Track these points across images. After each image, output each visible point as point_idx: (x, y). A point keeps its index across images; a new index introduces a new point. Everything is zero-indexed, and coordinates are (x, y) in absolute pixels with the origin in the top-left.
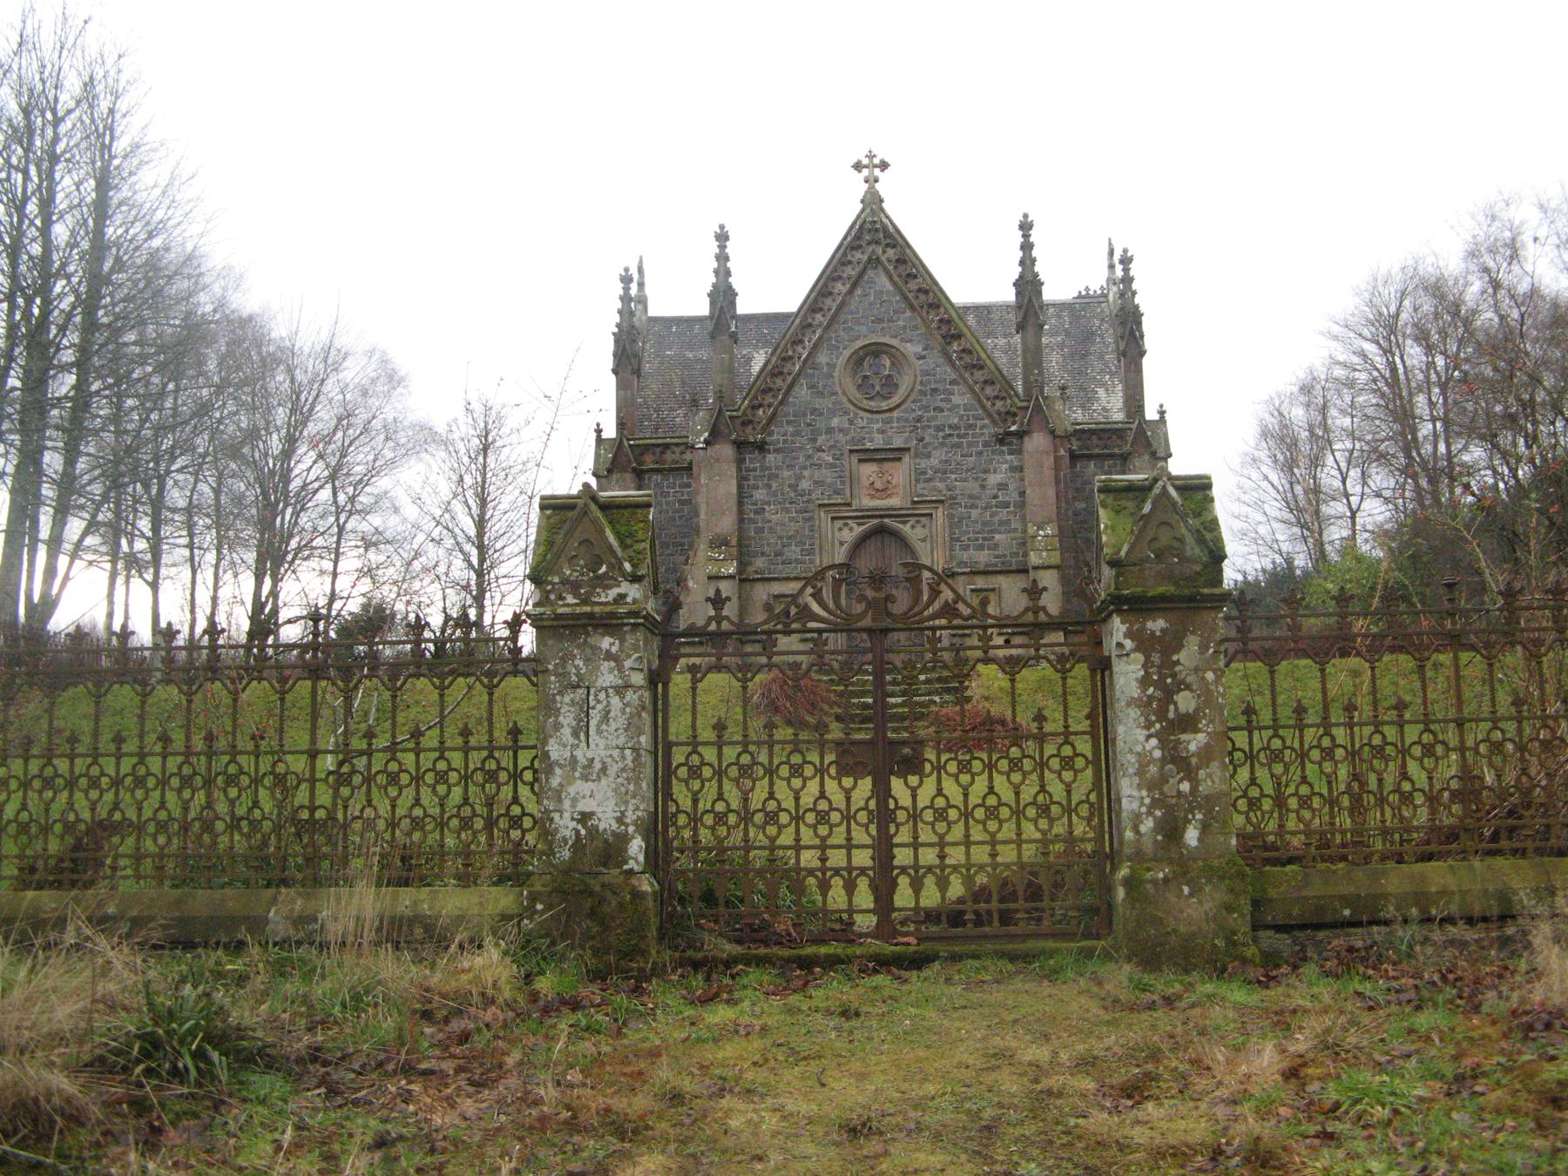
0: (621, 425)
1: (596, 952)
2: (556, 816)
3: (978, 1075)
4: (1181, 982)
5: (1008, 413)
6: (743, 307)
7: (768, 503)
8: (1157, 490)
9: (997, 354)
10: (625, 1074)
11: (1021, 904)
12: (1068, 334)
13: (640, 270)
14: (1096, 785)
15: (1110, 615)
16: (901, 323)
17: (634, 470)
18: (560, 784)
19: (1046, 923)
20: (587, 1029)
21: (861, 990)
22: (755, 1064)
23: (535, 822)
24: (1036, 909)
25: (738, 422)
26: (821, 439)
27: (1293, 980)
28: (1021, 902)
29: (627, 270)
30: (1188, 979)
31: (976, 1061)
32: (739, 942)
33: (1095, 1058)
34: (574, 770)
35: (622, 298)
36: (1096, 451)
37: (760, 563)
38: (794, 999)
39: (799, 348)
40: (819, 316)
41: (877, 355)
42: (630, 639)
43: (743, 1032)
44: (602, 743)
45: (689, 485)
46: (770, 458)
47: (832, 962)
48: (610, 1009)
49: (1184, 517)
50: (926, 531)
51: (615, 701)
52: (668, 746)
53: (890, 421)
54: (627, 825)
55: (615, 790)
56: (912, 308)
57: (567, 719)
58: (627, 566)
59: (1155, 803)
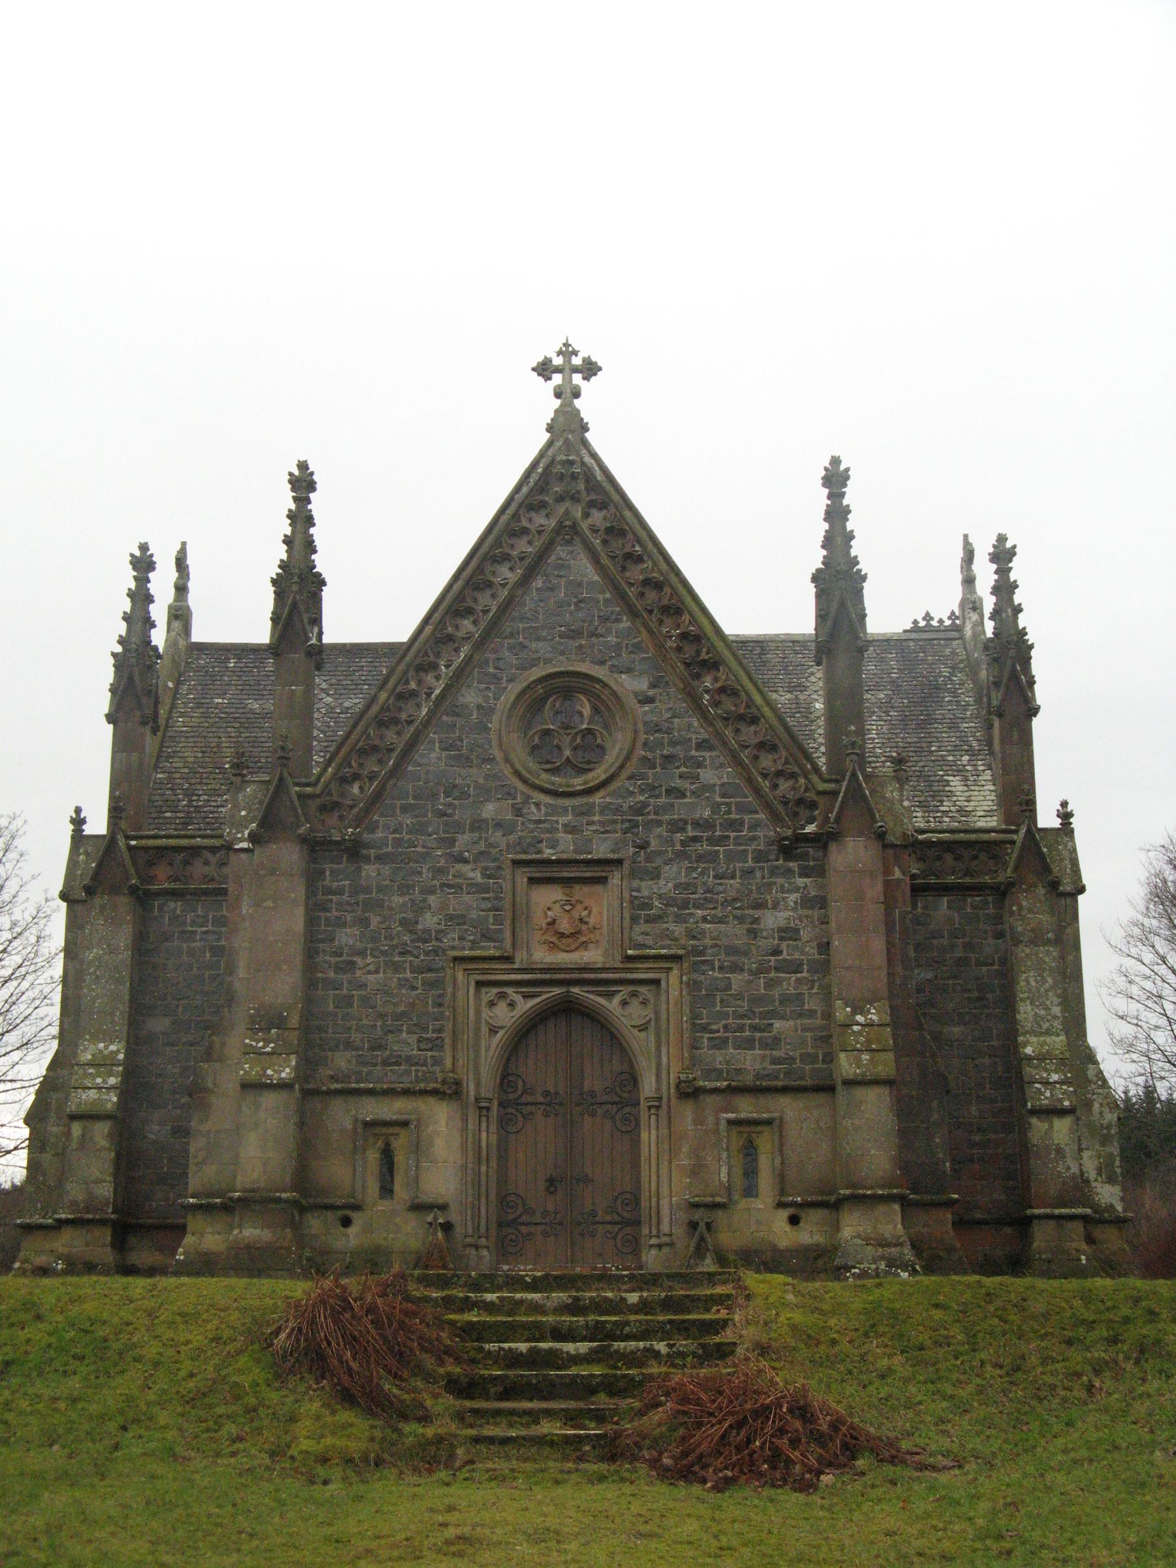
0: (116, 812)
5: (800, 802)
7: (362, 953)
12: (896, 686)
16: (612, 639)
17: (133, 890)
25: (313, 805)
26: (463, 840)
36: (951, 879)
37: (342, 1061)
39: (429, 678)
40: (467, 624)
41: (567, 693)
46: (370, 871)
50: (648, 1012)
53: (588, 811)
56: (633, 614)
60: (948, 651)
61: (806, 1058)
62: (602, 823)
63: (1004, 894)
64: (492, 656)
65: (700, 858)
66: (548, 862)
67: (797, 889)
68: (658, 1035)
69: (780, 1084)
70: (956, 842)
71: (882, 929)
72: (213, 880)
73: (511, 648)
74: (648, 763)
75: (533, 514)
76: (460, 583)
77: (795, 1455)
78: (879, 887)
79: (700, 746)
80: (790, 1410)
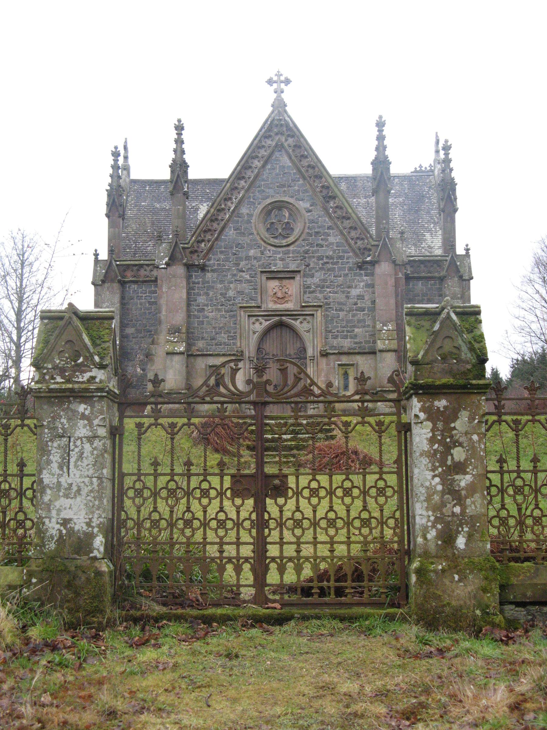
0: (111, 251)
1: (70, 611)
2: (47, 521)
3: (310, 701)
4: (451, 639)
5: (365, 249)
6: (192, 175)
8: (443, 315)
9: (360, 209)
10: (80, 697)
11: (349, 583)
13: (125, 148)
14: (400, 507)
15: (411, 396)
16: (296, 188)
17: (119, 281)
18: (50, 500)
19: (365, 596)
20: (60, 664)
21: (241, 639)
22: (166, 690)
23: (33, 524)
24: (360, 587)
25: (188, 251)
26: (242, 264)
27: (524, 640)
28: (349, 582)
29: (116, 148)
30: (455, 636)
31: (310, 691)
32: (164, 604)
33: (388, 691)
34: (59, 490)
35: (113, 167)
36: (423, 274)
37: (200, 344)
38: (197, 645)
39: (229, 203)
40: (242, 183)
41: (280, 209)
42: (98, 406)
43: (161, 667)
44: (78, 473)
45: (155, 292)
46: (209, 275)
47: (224, 620)
48: (76, 650)
49: (461, 333)
50: (310, 326)
51: (87, 447)
52: (122, 475)
53: (288, 252)
54: (93, 527)
55: (86, 505)
56: (304, 178)
57: (56, 457)
58: (97, 358)
59: (437, 520)
60: (428, 181)
61: (367, 342)
62: (293, 257)
63: (442, 280)
64: (252, 195)
65: (329, 270)
66: (274, 272)
67: (363, 281)
68: (313, 334)
69: (357, 351)
70: (425, 260)
71: (394, 296)
72: (148, 277)
73: (259, 192)
74: (310, 235)
75: (267, 140)
76: (239, 167)
77: (353, 464)
78: (393, 280)
79: (329, 228)
80: (352, 452)
